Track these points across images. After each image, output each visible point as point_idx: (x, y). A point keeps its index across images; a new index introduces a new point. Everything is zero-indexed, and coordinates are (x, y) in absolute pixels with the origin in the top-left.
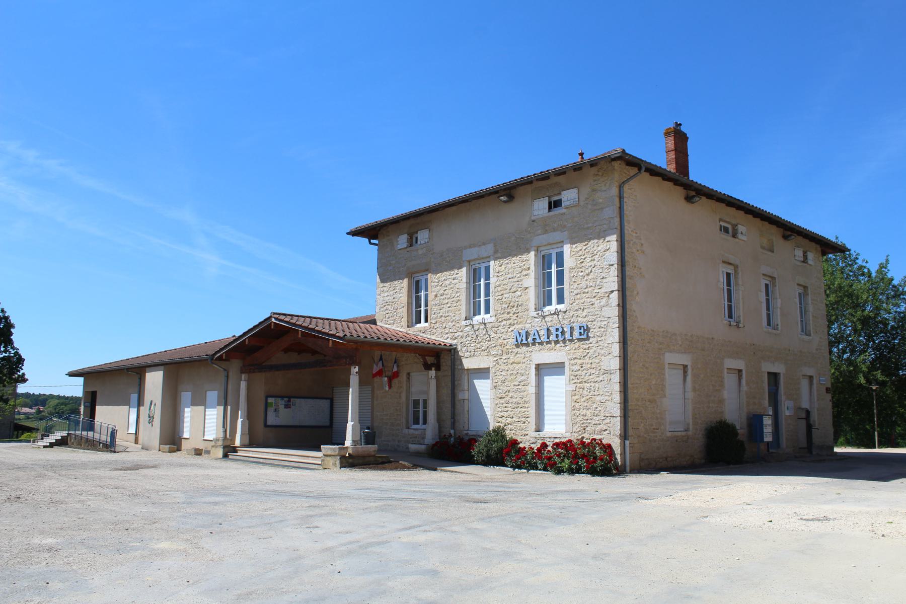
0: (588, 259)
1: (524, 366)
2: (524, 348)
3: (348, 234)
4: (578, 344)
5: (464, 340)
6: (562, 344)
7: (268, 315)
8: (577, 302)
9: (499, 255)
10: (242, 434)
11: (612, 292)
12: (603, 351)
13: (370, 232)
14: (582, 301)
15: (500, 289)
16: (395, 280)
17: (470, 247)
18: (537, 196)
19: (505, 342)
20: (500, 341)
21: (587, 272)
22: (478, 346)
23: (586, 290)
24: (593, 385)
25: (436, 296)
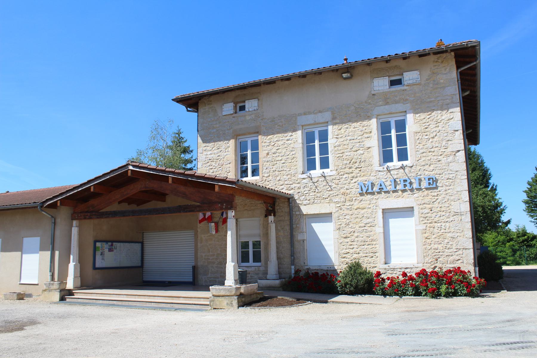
0: (432, 126)
2: (369, 196)
3: (173, 100)
4: (426, 192)
5: (302, 190)
6: (409, 192)
8: (423, 159)
9: (338, 121)
11: (458, 151)
12: (452, 198)
13: (192, 102)
15: (340, 148)
16: (220, 141)
19: (348, 191)
20: (342, 191)
21: (432, 135)
22: (318, 195)
23: (432, 150)
24: (443, 224)
25: (268, 154)
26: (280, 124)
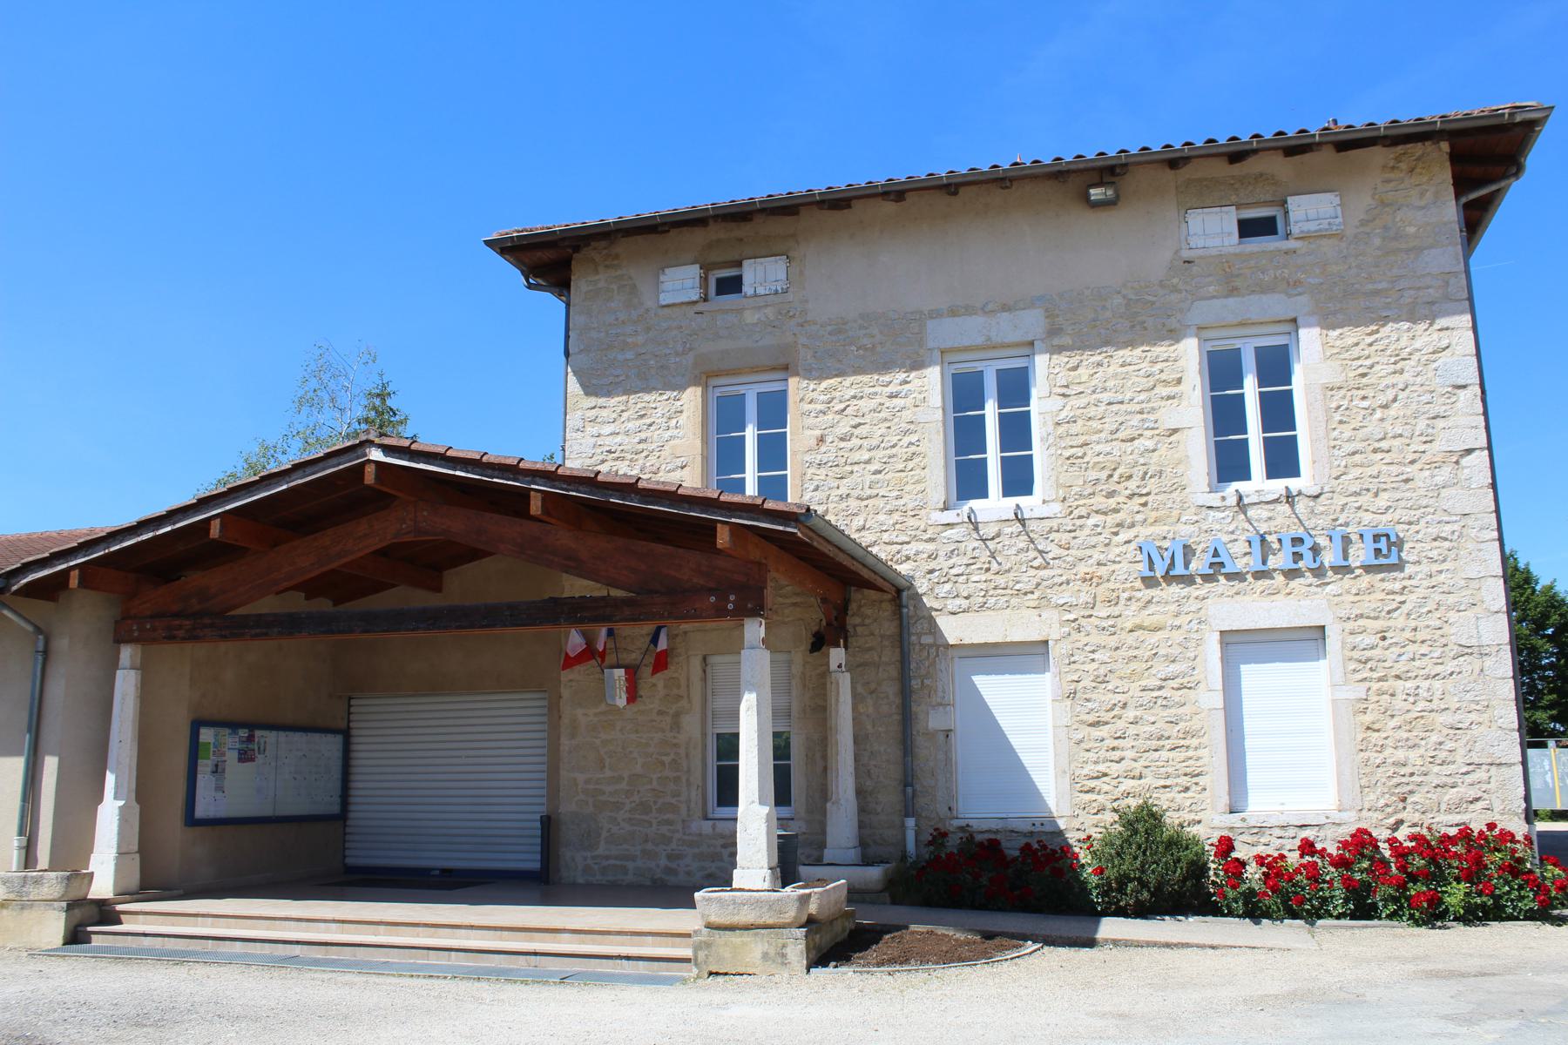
1: (1178, 636)
2: (1175, 590)
3: (488, 243)
4: (1366, 579)
5: (942, 563)
6: (1309, 578)
9: (1067, 340)
11: (1469, 451)
12: (1451, 599)
13: (548, 259)
14: (1374, 471)
16: (648, 390)
17: (953, 312)
18: (1203, 195)
19: (1103, 571)
21: (1382, 399)
23: (1384, 445)
24: (1425, 684)
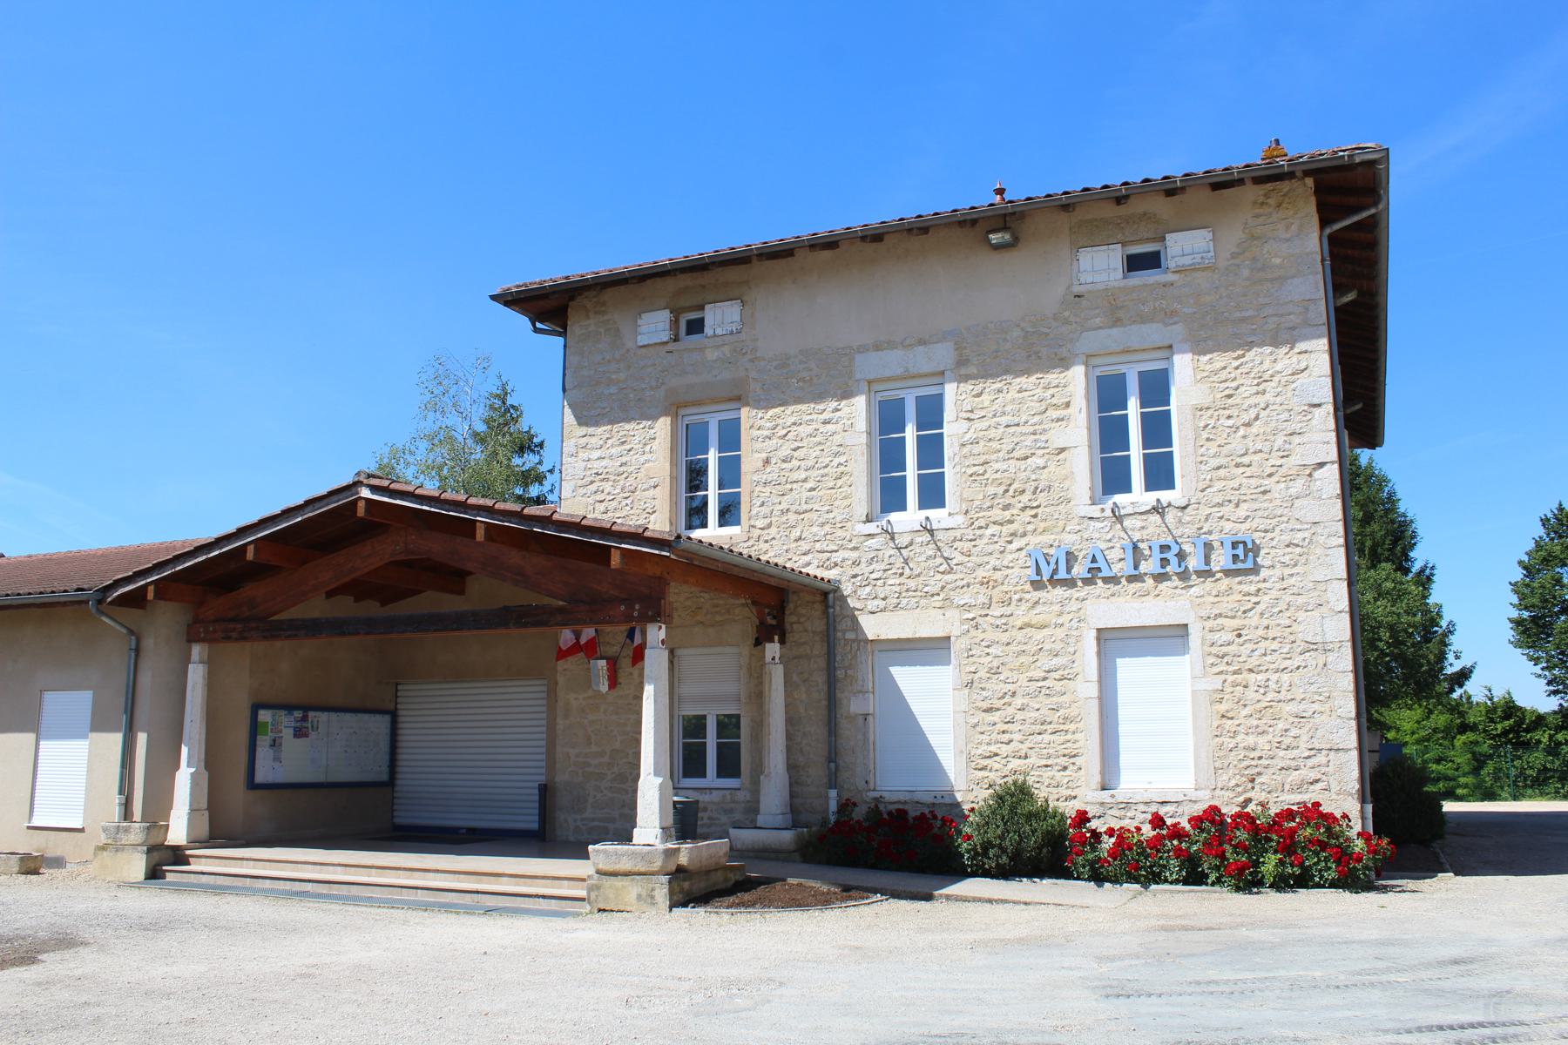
0: (1245, 391)
1: (1060, 633)
2: (1059, 592)
3: (493, 298)
4: (1226, 582)
5: (863, 568)
6: (1176, 582)
7: (347, 479)
8: (1219, 485)
9: (973, 370)
10: (193, 810)
11: (1321, 465)
12: (1300, 600)
15: (977, 449)
16: (628, 420)
17: (878, 347)
19: (998, 575)
21: (1246, 418)
22: (912, 584)
23: (1245, 460)
24: (1274, 677)
25: (767, 461)
26: (805, 374)
